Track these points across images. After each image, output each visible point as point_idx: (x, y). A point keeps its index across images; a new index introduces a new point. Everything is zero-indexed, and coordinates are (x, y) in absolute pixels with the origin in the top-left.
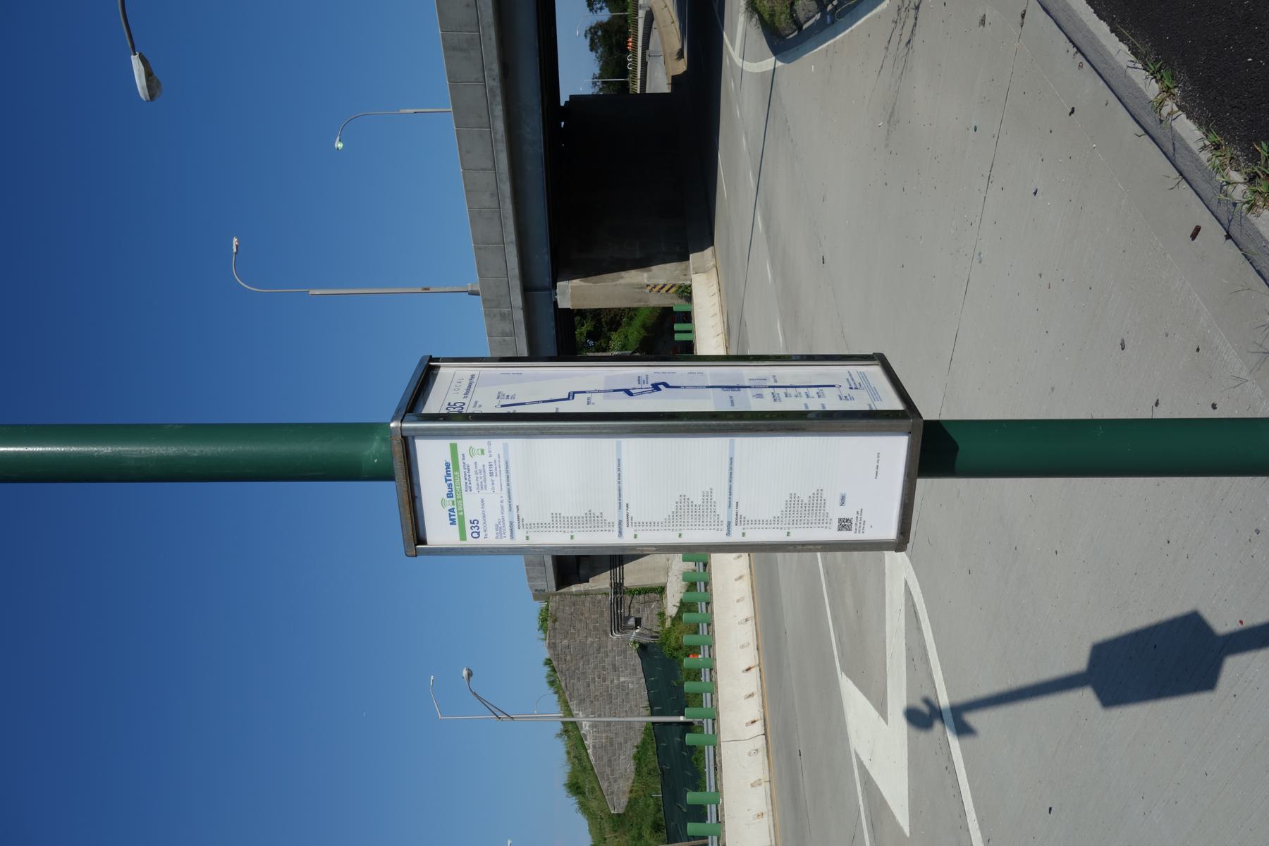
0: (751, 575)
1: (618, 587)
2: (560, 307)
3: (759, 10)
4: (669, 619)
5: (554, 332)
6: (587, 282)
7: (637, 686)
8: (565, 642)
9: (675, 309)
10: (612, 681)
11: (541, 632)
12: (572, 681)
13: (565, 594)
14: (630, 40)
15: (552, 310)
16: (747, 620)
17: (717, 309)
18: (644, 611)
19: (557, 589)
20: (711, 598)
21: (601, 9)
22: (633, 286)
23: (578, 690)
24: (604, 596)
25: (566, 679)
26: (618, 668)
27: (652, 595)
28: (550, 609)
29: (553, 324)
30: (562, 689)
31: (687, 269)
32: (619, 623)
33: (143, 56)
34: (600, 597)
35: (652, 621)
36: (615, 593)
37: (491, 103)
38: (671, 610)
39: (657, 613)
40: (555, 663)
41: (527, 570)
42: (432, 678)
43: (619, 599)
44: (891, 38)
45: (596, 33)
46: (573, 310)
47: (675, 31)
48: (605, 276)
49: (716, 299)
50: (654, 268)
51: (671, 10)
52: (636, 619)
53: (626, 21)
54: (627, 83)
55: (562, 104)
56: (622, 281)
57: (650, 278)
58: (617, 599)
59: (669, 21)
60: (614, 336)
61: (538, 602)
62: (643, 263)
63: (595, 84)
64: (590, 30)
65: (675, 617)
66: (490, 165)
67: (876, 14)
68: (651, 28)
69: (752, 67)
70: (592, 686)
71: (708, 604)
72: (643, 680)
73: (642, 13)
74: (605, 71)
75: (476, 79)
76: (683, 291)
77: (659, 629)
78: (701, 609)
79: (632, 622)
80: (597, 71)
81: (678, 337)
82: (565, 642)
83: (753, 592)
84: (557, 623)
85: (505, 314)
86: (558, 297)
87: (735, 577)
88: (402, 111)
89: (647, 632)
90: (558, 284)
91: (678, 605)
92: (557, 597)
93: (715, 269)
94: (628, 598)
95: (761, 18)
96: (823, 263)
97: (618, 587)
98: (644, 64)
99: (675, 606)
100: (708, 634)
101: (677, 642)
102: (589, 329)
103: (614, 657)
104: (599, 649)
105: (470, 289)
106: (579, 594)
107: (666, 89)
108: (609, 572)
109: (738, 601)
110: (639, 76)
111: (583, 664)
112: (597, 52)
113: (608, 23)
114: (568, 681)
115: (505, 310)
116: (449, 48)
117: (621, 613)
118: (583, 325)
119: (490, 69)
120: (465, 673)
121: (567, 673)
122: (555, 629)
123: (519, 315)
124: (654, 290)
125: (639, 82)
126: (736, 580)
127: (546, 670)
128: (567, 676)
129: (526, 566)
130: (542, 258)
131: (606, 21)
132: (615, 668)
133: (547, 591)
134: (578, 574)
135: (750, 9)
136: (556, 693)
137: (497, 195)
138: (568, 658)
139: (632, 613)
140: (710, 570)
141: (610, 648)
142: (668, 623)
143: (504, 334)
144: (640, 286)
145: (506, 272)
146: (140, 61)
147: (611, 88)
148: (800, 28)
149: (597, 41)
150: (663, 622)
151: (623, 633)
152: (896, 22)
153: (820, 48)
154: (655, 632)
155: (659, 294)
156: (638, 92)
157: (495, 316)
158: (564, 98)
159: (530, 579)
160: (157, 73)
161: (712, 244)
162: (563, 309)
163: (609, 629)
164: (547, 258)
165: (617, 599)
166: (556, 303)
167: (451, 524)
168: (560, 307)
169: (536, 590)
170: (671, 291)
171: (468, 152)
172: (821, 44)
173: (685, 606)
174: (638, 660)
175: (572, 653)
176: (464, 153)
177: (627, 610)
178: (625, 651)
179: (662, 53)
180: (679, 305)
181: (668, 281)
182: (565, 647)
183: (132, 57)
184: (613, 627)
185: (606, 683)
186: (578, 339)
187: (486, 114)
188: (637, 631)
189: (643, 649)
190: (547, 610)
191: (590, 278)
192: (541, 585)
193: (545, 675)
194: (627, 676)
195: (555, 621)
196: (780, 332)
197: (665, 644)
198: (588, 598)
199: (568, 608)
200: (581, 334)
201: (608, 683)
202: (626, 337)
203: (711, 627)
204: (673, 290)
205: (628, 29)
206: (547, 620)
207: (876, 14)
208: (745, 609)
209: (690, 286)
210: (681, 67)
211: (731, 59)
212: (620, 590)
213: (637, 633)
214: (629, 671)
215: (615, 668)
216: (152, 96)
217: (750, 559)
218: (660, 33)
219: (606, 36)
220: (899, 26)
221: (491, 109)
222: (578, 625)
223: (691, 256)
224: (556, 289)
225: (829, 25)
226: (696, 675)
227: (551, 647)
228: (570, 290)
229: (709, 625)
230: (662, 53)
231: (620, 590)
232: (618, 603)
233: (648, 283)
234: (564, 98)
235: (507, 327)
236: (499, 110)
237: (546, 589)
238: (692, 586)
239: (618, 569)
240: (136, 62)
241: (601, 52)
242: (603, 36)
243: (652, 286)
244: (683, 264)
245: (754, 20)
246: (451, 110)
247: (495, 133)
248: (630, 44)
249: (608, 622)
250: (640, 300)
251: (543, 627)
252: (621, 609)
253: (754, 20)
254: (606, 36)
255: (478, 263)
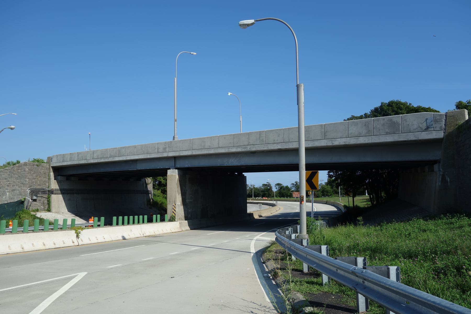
0: (45, 249)
1: (51, 192)
2: (168, 170)
3: (271, 246)
4: (35, 214)
5: (158, 168)
6: (177, 180)
7: (4, 200)
8: (27, 170)
9: (166, 215)
10: (7, 189)
11: (33, 160)
12: (8, 172)
13: (50, 170)
14: (266, 198)
15: (167, 167)
16: (23, 248)
17: (165, 232)
18: (40, 203)
19: (52, 167)
20: (35, 232)
21: (276, 188)
22: (175, 198)
23: (4, 174)
24: (48, 186)
25: (9, 169)
26: (13, 192)
27: (47, 206)
28: (43, 163)
29: (162, 168)
30: (5, 168)
31: (182, 220)
32: (34, 192)
33: (254, 24)
34: (47, 184)
35: (35, 206)
36: (49, 191)
37: (241, 147)
38: (39, 215)
39: (38, 208)
40: (17, 165)
41: (61, 154)
42: (15, 114)
43: (46, 192)
44: (255, 303)
45: (269, 186)
46: (167, 176)
47: (267, 214)
48: (179, 188)
49: (169, 231)
50: (182, 207)
51: (275, 213)
52: (36, 199)
53: (272, 197)
54: (252, 197)
55: (243, 173)
56: (177, 194)
57: (178, 205)
58: (46, 192)
59: (272, 212)
60: (159, 191)
61: (47, 159)
62: (184, 203)
63: (252, 186)
64: (269, 184)
65: (35, 216)
66: (220, 146)
67: (265, 296)
68: (270, 206)
69: (253, 242)
70: (5, 180)
71: (33, 230)
72: (6, 202)
73: (274, 202)
74: (256, 189)
75: (250, 142)
76: (173, 218)
77: (31, 209)
78: (19, 229)
79: (35, 198)
80: (256, 187)
81: (154, 216)
82: (27, 170)
83: (36, 250)
84: (36, 166)
85: (166, 149)
86: (172, 170)
87: (45, 242)
88: (241, 117)
89: (29, 204)
90: (177, 170)
91: (41, 217)
92: (49, 167)
93: (181, 231)
94: (46, 196)
95: (269, 247)
96: (171, 278)
97: (51, 192)
98: (257, 203)
99: (41, 216)
100: (18, 231)
101: (23, 217)
102: (162, 182)
103: (19, 190)
104: (23, 184)
105: (175, 136)
106: (49, 176)
107: (249, 211)
108: (59, 188)
109: (33, 244)
110: (254, 201)
111: (16, 177)
112: (262, 186)
113: (272, 191)
114: (8, 170)
115: (167, 150)
116: (260, 133)
117: (39, 193)
118: (164, 180)
119: (253, 147)
120: (13, 127)
121: (13, 170)
122: (33, 165)
123: (165, 155)
124: (174, 207)
125: (252, 201)
126: (43, 243)
127: (15, 161)
128: (11, 170)
129: (63, 154)
130: (187, 164)
131: (272, 190)
132: (13, 190)
133: (51, 162)
134: (59, 176)
135: (272, 242)
136: (4, 165)
137: (209, 148)
138: (19, 171)
139: (39, 198)
140: (49, 231)
141: (23, 188)
142: (33, 213)
143: (158, 149)
144: (175, 201)
145: (181, 150)
146: (252, 22)
147: (250, 191)
148: (264, 263)
149: (266, 187)
150: (34, 211)
151: (30, 194)
152: (260, 305)
153: (255, 271)
154: (29, 208)
155: (172, 209)
156: (247, 201)
157: (165, 146)
158: (245, 174)
159: (57, 156)
160: (248, 28)
161: (191, 229)
162: (167, 172)
163: (32, 188)
164: (187, 166)
165: (46, 192)
166: (169, 169)
167: (296, 182)
168: (168, 170)
169: (52, 158)
170: (173, 213)
171: (225, 138)
172: (256, 272)
173: (42, 221)
174: (16, 200)
175: (22, 172)
176: (225, 137)
177: (40, 196)
178: (21, 195)
179: (261, 209)
180: (167, 217)
181: (177, 212)
182: (25, 170)
183: (254, 20)
184: (33, 190)
185: (6, 187)
186: (158, 177)
187: (238, 145)
188: (30, 200)
189: (22, 202)
190: (43, 163)
191: (179, 182)
192: (54, 160)
193: (13, 161)
194: (9, 196)
195: (37, 166)
196: (148, 259)
197: (23, 212)
198: (47, 180)
199: (43, 171)
200: (160, 179)
201: (6, 187)
202: (159, 196)
203: (21, 232)
204: (174, 214)
205: (270, 197)
206: (38, 162)
207: (264, 296)
208: (28, 247)
209: (175, 221)
210: (256, 217)
211: (257, 235)
212: (50, 193)
213: (29, 200)
214: (11, 196)
215: (13, 190)
216: (240, 25)
217: (53, 248)
218: (268, 209)
219: (268, 190)
220: (259, 307)
221: (240, 147)
222: (35, 175)
223: (187, 221)
224: (175, 169)
225: (263, 275)
226: (21, 224)
227: (25, 164)
228: (174, 174)
229: (22, 231)
230: (261, 209)
231: (50, 193)
232: (44, 192)
233: (176, 205)
234: (245, 174)
235: (161, 150)
236: (239, 150)
237: (52, 162)
238: (51, 224)
239: (60, 192)
240: (252, 21)
241: (262, 188)
242: (267, 189)
243: (175, 206)
244: (183, 218)
245: (268, 244)
246: (241, 133)
247: (231, 148)
248: (265, 198)
249: (35, 188)
250: (170, 201)
251: (35, 160)
252: (41, 193)
253: (268, 244)
254: (268, 190)
255: (185, 140)
